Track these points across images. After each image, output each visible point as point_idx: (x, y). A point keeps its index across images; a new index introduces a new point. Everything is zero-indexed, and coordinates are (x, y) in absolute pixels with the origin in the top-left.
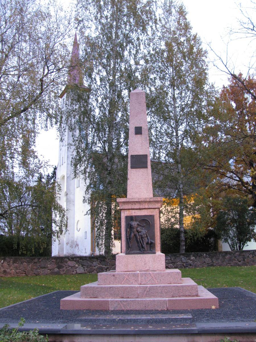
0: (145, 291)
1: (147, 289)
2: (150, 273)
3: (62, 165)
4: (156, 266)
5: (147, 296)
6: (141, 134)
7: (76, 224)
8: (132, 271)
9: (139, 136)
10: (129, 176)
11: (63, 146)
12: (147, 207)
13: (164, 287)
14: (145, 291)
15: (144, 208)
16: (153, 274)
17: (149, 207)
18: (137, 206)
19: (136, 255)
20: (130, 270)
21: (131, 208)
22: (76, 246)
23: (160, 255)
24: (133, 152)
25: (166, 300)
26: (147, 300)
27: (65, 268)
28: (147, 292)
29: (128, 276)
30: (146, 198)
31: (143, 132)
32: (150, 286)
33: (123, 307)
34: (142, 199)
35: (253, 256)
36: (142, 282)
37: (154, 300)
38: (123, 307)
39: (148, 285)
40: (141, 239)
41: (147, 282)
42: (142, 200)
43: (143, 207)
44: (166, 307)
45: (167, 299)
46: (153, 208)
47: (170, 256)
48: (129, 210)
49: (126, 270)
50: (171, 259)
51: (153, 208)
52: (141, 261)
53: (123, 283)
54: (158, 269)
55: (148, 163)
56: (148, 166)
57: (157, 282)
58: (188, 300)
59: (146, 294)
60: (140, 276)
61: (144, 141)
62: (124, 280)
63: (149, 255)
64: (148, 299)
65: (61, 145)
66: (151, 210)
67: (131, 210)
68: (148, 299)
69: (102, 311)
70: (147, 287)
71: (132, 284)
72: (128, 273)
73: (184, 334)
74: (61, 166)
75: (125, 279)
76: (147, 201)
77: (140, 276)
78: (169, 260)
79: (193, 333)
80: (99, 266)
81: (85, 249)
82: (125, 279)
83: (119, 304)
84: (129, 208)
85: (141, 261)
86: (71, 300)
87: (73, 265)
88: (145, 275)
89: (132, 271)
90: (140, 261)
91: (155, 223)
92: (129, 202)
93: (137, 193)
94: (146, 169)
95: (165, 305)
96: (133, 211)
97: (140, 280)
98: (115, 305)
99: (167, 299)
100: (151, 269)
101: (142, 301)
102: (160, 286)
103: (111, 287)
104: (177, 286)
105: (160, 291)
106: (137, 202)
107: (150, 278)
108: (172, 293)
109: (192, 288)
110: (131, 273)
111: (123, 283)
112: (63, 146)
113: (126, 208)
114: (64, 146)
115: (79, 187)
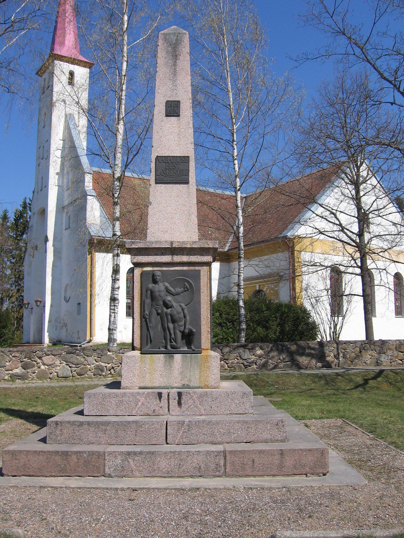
3: (41, 190)
6: (179, 116)
7: (63, 290)
10: (151, 199)
11: (42, 159)
22: (62, 326)
27: (36, 368)
46: (116, 416)
51: (116, 416)
56: (190, 179)
62: (138, 406)
65: (40, 157)
69: (163, 329)
73: (120, 106)
74: (40, 192)
75: (140, 403)
80: (97, 363)
81: (78, 332)
82: (140, 403)
87: (50, 363)
93: (167, 232)
112: (42, 159)
114: (44, 159)
115: (69, 228)
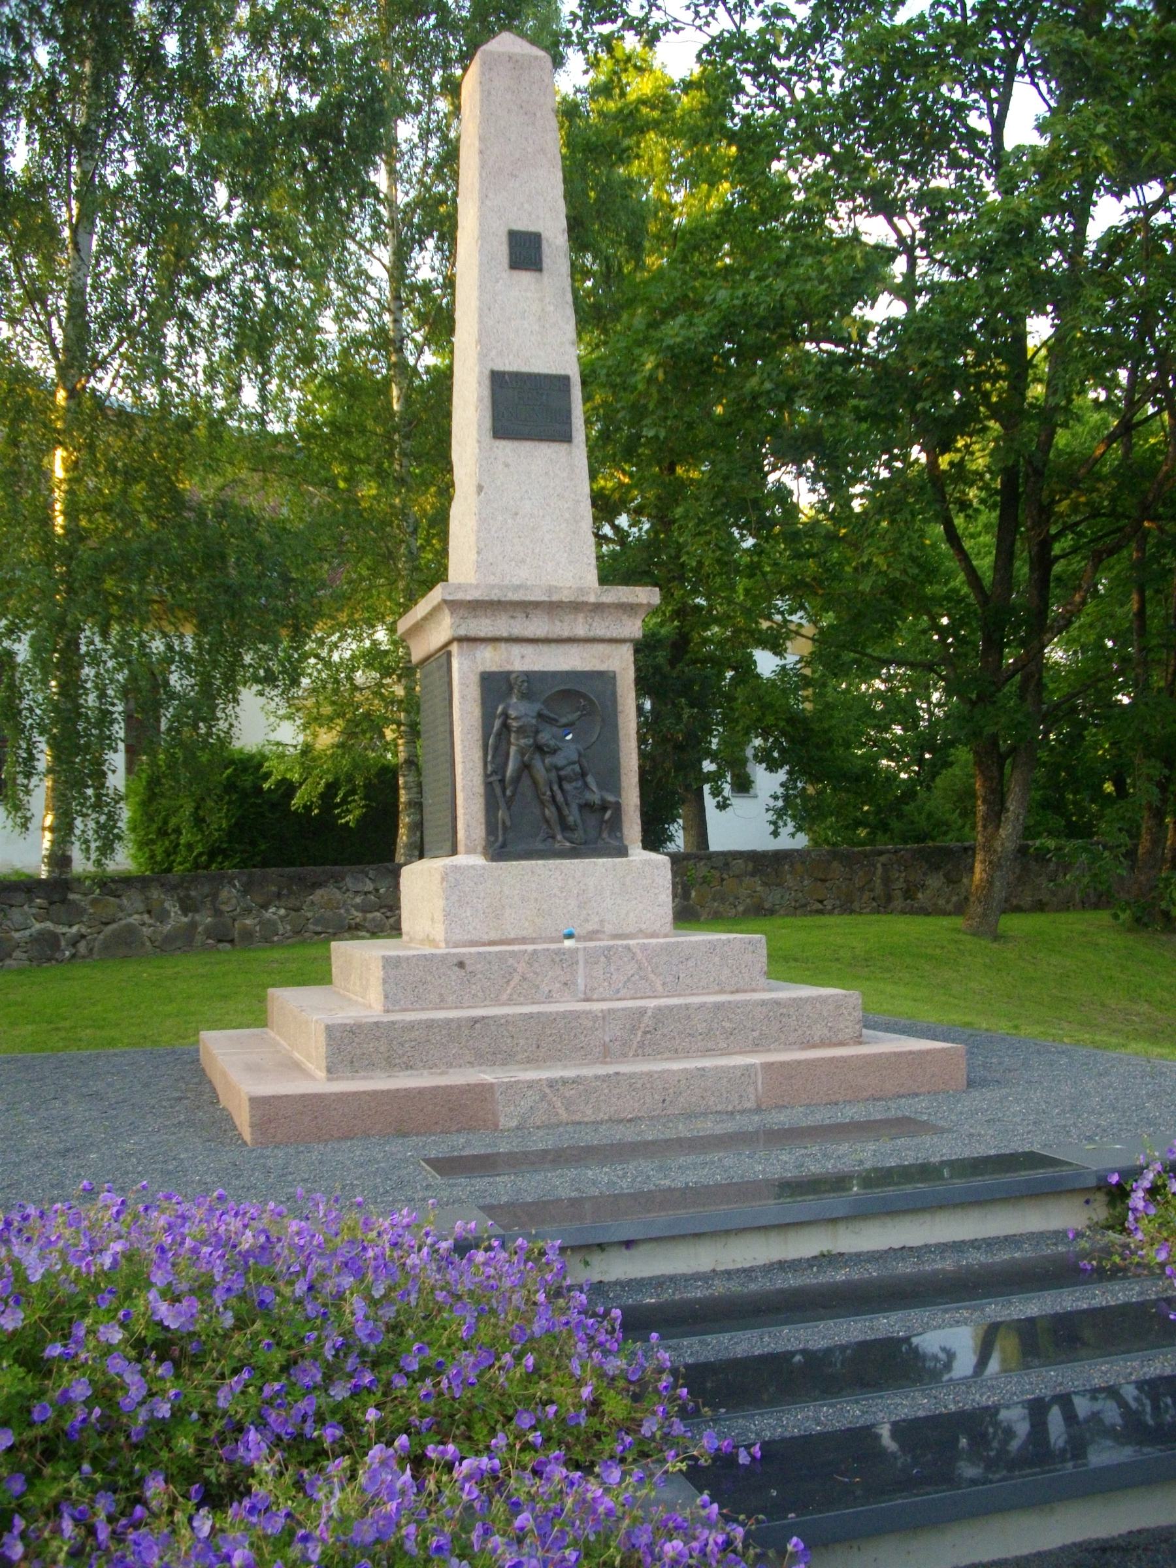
0: (633, 1029)
1: (646, 1019)
2: (628, 948)
4: (632, 915)
5: (643, 1051)
8: (523, 941)
9: (525, 278)
12: (581, 631)
13: (718, 1007)
14: (633, 1029)
15: (571, 635)
16: (644, 948)
17: (591, 634)
18: (537, 627)
19: (540, 862)
20: (512, 936)
21: (505, 634)
23: (646, 863)
24: (500, 353)
25: (753, 1065)
26: (674, 1072)
28: (645, 1033)
29: (530, 964)
30: (581, 589)
31: (547, 262)
32: (659, 1009)
33: (562, 1111)
34: (566, 592)
35: (723, 880)
36: (593, 989)
37: (703, 1069)
38: (562, 1111)
39: (652, 1003)
40: (556, 787)
41: (618, 991)
42: (565, 596)
43: (566, 634)
44: (752, 1097)
45: (755, 1060)
47: (371, 874)
48: (498, 645)
49: (494, 935)
50: (377, 890)
52: (561, 889)
53: (505, 997)
54: (644, 927)
55: (574, 420)
57: (660, 988)
58: (844, 1060)
59: (641, 1045)
60: (581, 963)
61: (552, 308)
62: (512, 984)
63: (601, 861)
64: (675, 1066)
66: (601, 647)
67: (503, 645)
68: (675, 1066)
70: (642, 1012)
71: (549, 998)
72: (530, 948)
75: (517, 978)
76: (586, 604)
77: (581, 963)
78: (366, 893)
79: (1077, 1185)
82: (517, 978)
83: (544, 1097)
84: (498, 634)
85: (561, 889)
86: (303, 1096)
88: (608, 952)
89: (523, 941)
90: (556, 891)
91: (620, 708)
92: (499, 602)
93: (523, 561)
94: (565, 446)
95: (751, 1089)
96: (516, 650)
97: (581, 981)
98: (525, 1104)
99: (755, 1060)
100: (608, 928)
101: (650, 1074)
102: (702, 1006)
103: (475, 1021)
104: (777, 1003)
105: (702, 1027)
106: (536, 605)
107: (631, 968)
108: (756, 1034)
109: (839, 1007)
110: (539, 947)
111: (505, 997)
113: (482, 635)
